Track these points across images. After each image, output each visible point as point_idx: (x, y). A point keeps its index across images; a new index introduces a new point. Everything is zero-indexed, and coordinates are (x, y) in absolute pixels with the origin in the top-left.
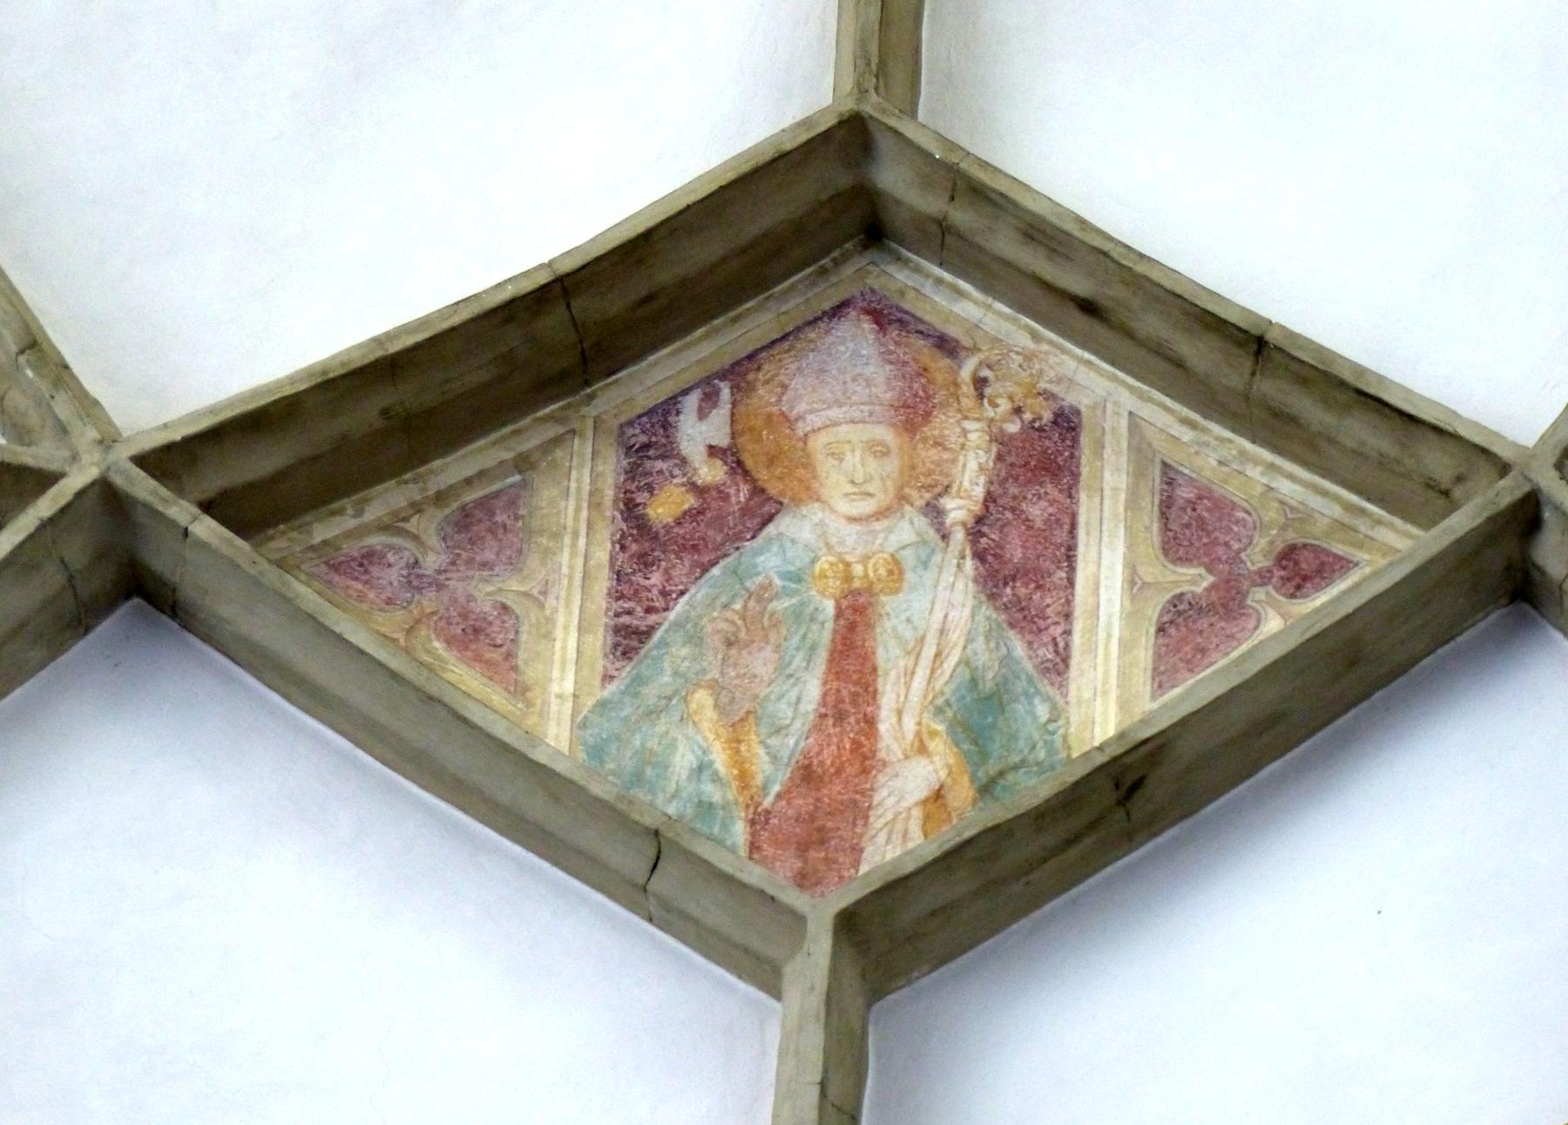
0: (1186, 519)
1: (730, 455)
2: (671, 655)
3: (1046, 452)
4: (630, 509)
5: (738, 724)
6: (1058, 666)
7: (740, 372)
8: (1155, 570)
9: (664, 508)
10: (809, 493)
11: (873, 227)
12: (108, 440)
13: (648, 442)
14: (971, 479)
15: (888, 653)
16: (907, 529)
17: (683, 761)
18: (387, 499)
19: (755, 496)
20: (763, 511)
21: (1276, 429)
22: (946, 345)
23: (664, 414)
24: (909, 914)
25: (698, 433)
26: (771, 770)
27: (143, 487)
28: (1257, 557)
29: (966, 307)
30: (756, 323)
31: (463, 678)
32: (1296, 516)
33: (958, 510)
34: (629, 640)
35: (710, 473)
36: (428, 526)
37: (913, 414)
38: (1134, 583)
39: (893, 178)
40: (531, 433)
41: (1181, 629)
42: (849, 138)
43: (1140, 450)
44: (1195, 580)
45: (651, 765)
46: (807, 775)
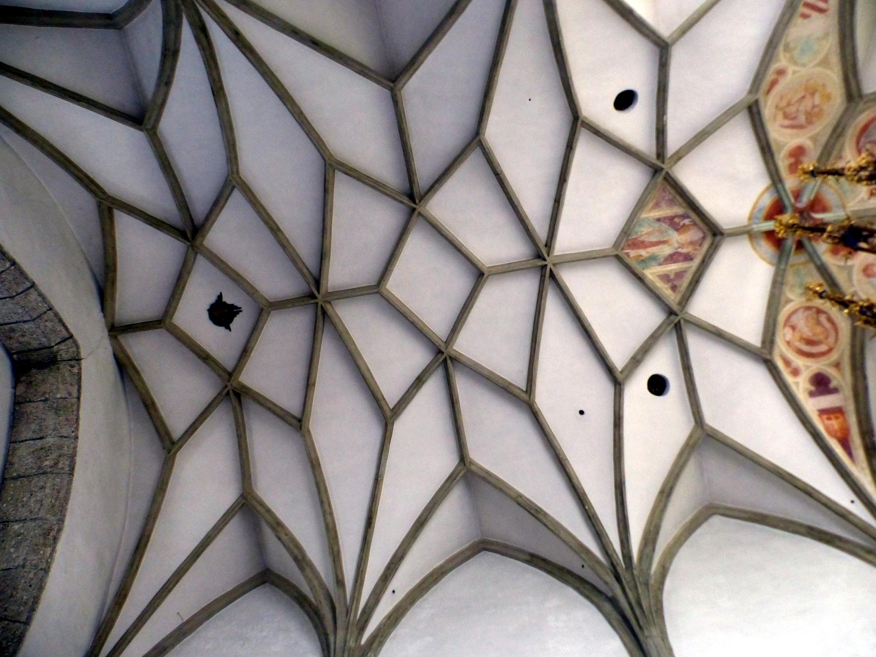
0: (680, 275)
1: (684, 225)
2: (657, 225)
3: (688, 258)
4: (676, 216)
5: (648, 234)
6: (660, 264)
7: (695, 224)
8: (673, 272)
9: (677, 220)
10: (680, 234)
11: (714, 235)
12: (670, 168)
13: (684, 216)
14: (684, 251)
15: (659, 247)
16: (676, 245)
17: (643, 229)
18: (672, 191)
19: (679, 229)
20: (677, 230)
21: (690, 283)
22: (701, 245)
23: (688, 217)
24: (295, 594)
25: (687, 221)
26: (642, 239)
27: (664, 173)
28: (675, 283)
29: (706, 245)
30: (701, 225)
31: (651, 205)
32: (681, 286)
33: (680, 250)
34: (659, 220)
35: (682, 224)
36: (671, 197)
37: (692, 243)
38: (671, 271)
39: (718, 238)
40: (684, 204)
41: (665, 278)
42: (722, 234)
43: (689, 268)
44: (672, 276)
45: (641, 225)
46: (643, 242)
